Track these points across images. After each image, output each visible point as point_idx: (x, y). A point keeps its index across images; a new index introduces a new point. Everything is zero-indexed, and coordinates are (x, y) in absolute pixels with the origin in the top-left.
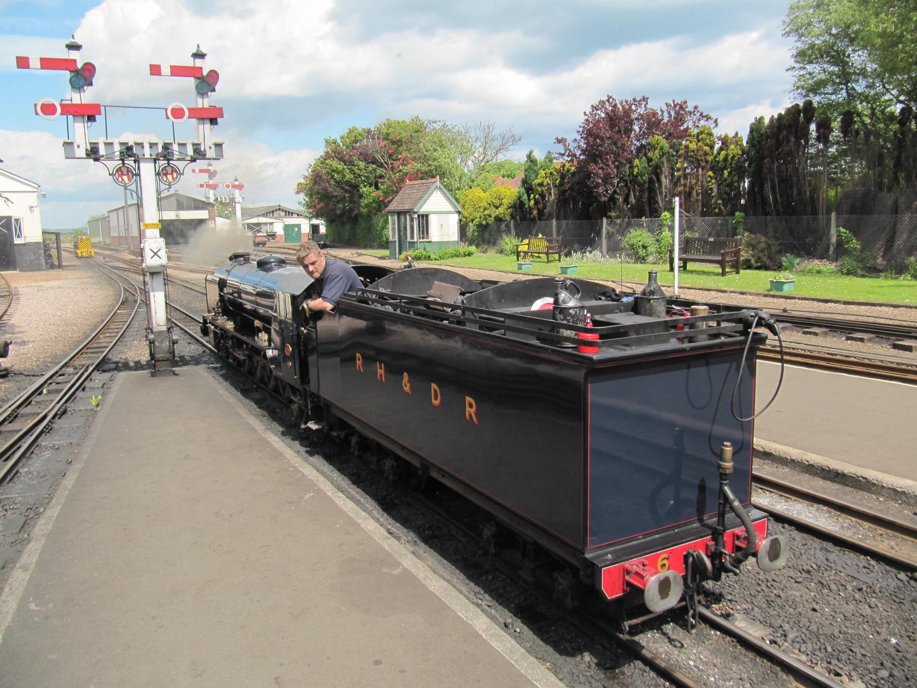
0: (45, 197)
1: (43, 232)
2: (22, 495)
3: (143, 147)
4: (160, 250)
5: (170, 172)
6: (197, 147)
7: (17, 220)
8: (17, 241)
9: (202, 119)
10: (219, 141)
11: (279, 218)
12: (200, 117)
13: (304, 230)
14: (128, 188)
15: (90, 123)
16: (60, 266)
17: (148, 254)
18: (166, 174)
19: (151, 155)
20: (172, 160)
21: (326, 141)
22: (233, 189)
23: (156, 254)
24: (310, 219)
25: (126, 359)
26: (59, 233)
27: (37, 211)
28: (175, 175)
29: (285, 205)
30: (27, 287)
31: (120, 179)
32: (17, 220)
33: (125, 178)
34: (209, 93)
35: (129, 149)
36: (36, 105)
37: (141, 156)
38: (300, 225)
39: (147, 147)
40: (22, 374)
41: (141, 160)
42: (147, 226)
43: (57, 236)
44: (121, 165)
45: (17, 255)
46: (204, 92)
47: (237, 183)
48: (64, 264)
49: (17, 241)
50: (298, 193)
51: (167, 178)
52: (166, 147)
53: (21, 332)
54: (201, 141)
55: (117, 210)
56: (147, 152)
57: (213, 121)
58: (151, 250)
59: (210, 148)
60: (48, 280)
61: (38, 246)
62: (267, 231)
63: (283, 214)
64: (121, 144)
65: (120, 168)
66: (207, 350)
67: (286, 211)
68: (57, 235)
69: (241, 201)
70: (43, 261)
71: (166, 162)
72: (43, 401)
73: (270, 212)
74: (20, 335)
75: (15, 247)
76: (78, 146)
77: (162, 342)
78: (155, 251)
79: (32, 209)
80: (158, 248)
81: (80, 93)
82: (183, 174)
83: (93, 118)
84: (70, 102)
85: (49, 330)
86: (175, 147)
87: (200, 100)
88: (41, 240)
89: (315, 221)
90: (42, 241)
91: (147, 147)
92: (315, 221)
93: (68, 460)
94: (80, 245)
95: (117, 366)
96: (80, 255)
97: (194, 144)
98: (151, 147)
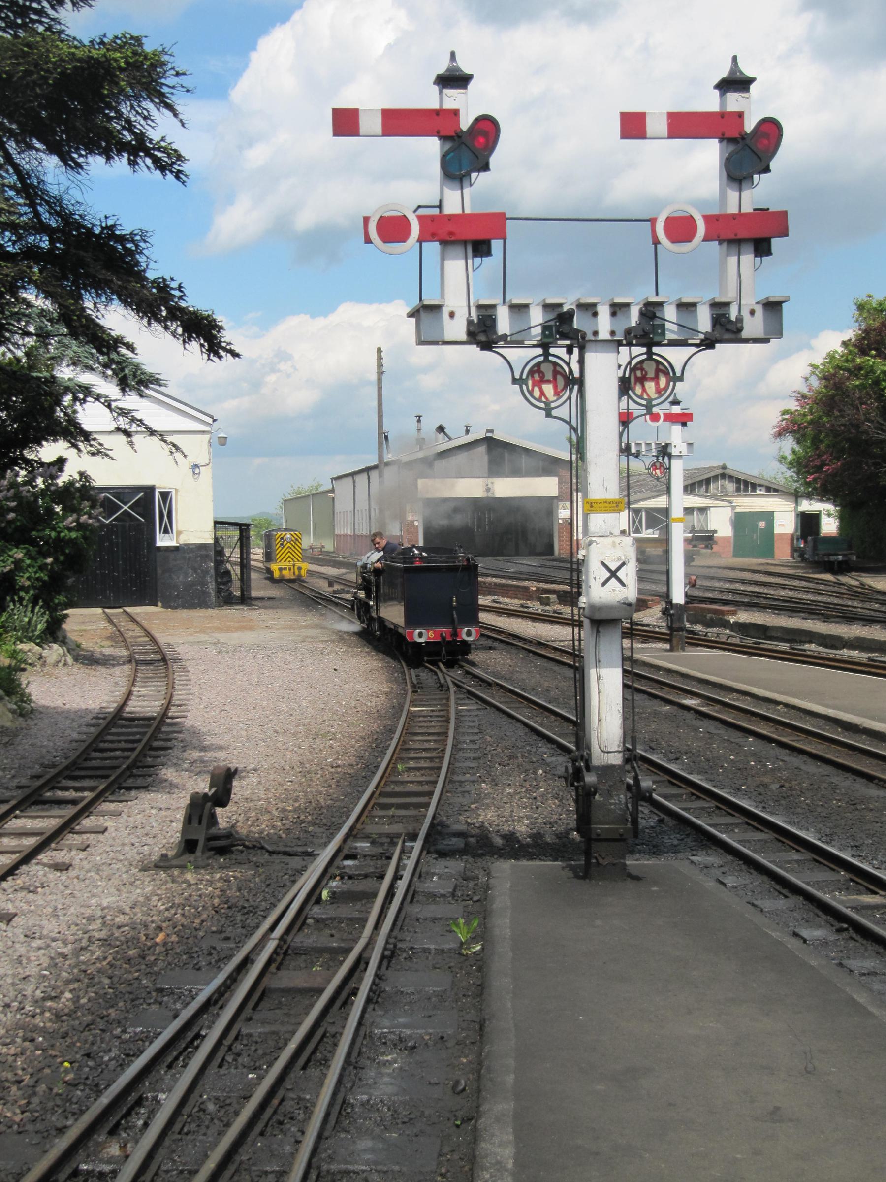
0: (224, 444)
1: (216, 522)
2: (379, 1168)
3: (595, 314)
4: (623, 564)
5: (651, 374)
6: (719, 309)
7: (165, 495)
8: (162, 541)
9: (734, 243)
10: (775, 296)
11: (722, 496)
12: (732, 237)
13: (783, 525)
14: (554, 413)
15: (478, 260)
16: (245, 600)
17: (595, 574)
18: (642, 380)
19: (613, 333)
20: (659, 344)
21: (861, 307)
22: (668, 423)
23: (613, 574)
24: (796, 496)
25: (482, 826)
26: (248, 525)
27: (206, 474)
28: (663, 381)
29: (738, 467)
30: (192, 643)
31: (537, 392)
32: (165, 495)
33: (548, 389)
34: (756, 177)
35: (565, 318)
36: (366, 220)
37: (590, 337)
38: (772, 514)
39: (604, 312)
40: (262, 848)
41: (588, 346)
42: (592, 506)
43: (241, 531)
44: (541, 358)
45: (159, 571)
46: (745, 173)
47: (676, 409)
48: (254, 594)
49: (162, 541)
50: (780, 434)
51: (644, 390)
52: (651, 311)
53: (220, 748)
54: (730, 295)
55: (353, 474)
56: (604, 324)
57: (762, 248)
58: (603, 564)
59: (752, 313)
60: (229, 630)
61: (203, 552)
62: (693, 527)
63: (730, 486)
64: (547, 307)
65: (538, 365)
66: (667, 819)
67: (738, 481)
68: (244, 529)
69: (685, 452)
70: (211, 587)
71: (644, 350)
72: (332, 919)
73: (700, 483)
74: (219, 754)
75: (158, 554)
76: (452, 315)
77: (609, 794)
78: (613, 569)
79: (197, 471)
80: (619, 559)
81: (462, 189)
82: (681, 379)
83: (485, 247)
84: (436, 211)
85: (279, 745)
86: (670, 313)
87: (733, 195)
88: (211, 541)
89: (806, 506)
90: (212, 541)
91: (604, 312)
92: (806, 506)
93: (457, 1083)
94: (279, 552)
95: (467, 844)
96: (277, 575)
97: (714, 305)
98: (613, 314)
